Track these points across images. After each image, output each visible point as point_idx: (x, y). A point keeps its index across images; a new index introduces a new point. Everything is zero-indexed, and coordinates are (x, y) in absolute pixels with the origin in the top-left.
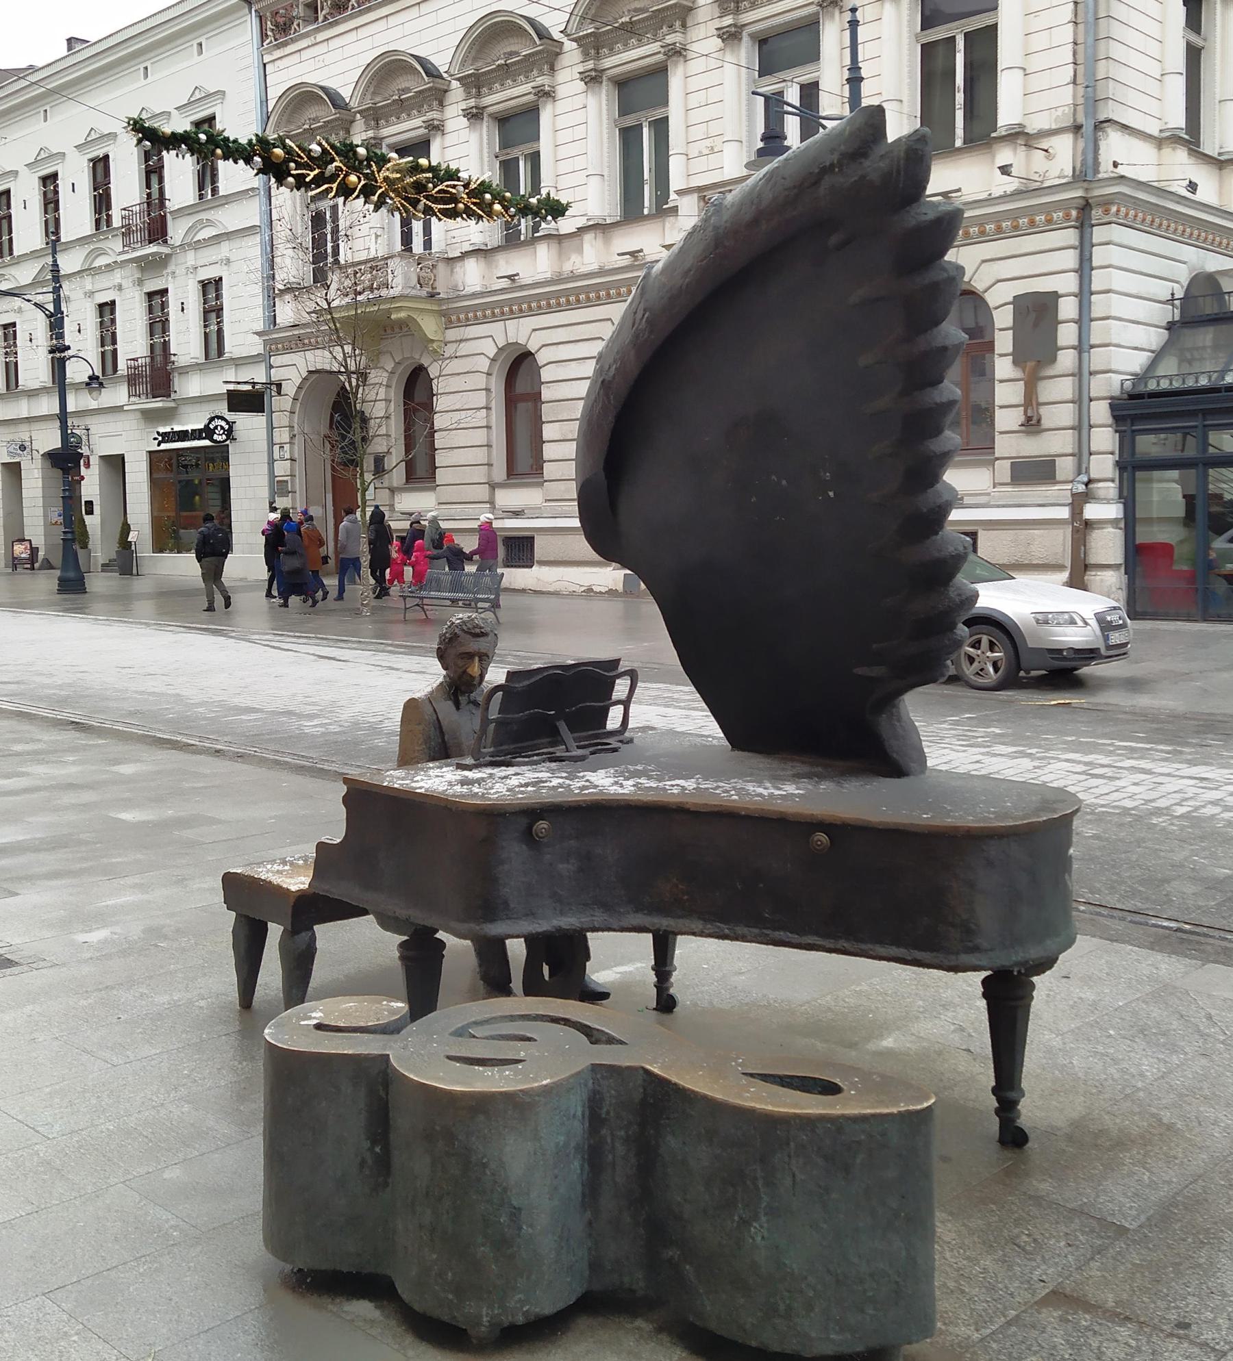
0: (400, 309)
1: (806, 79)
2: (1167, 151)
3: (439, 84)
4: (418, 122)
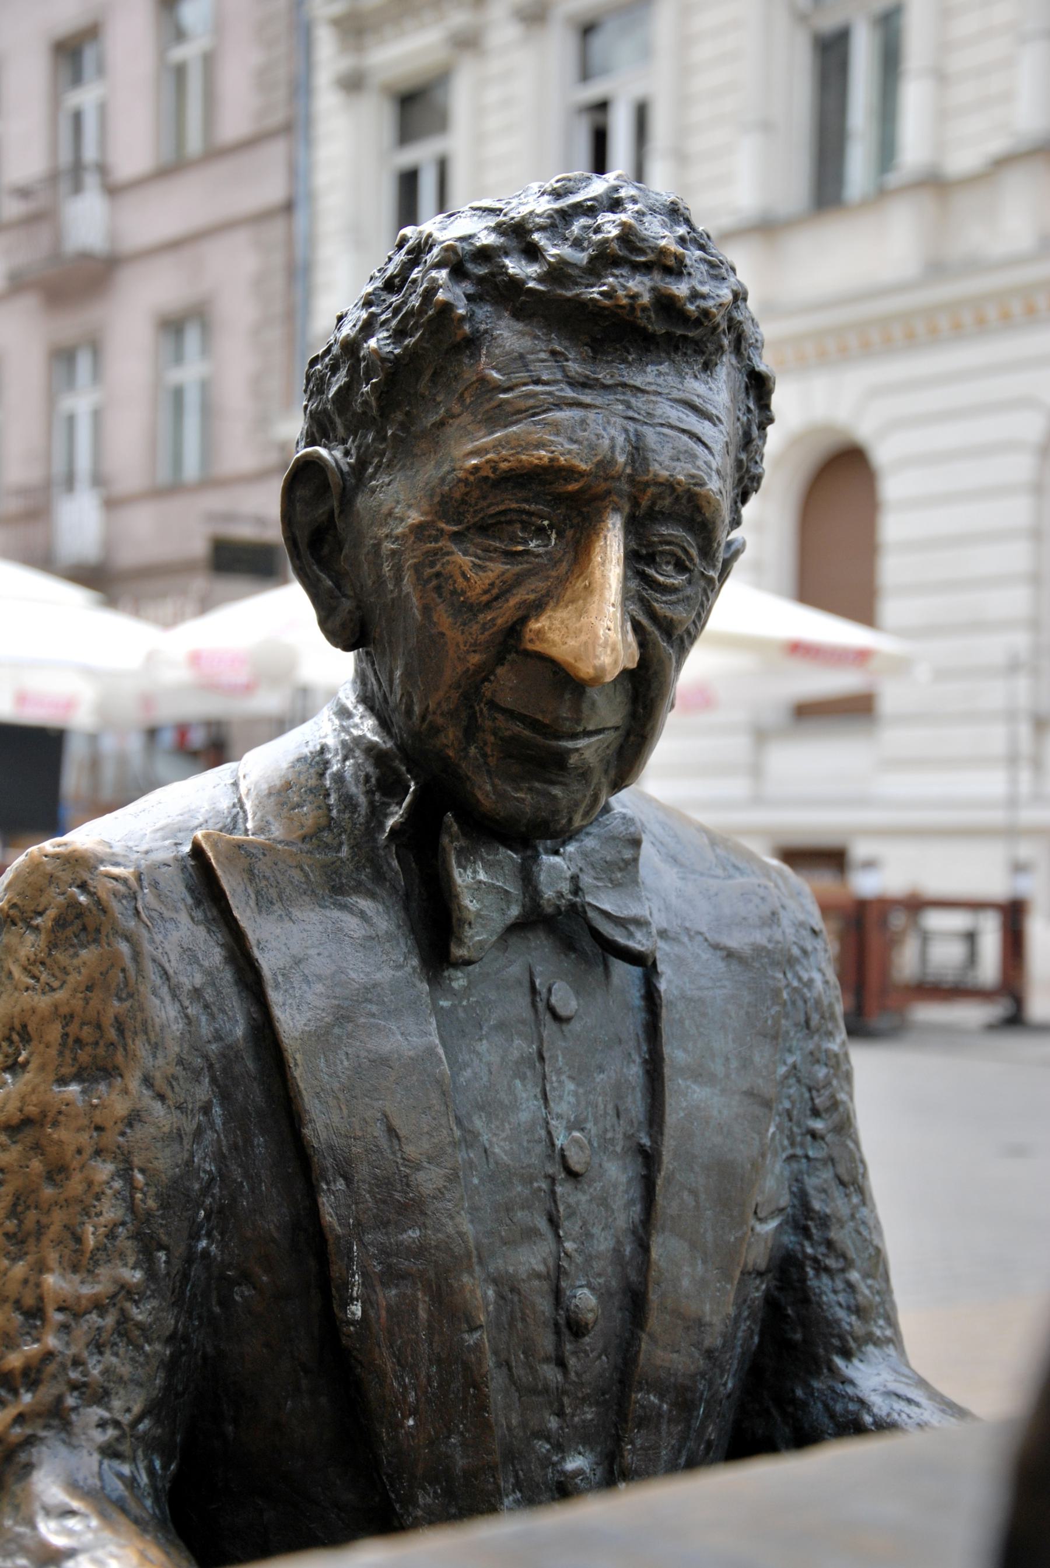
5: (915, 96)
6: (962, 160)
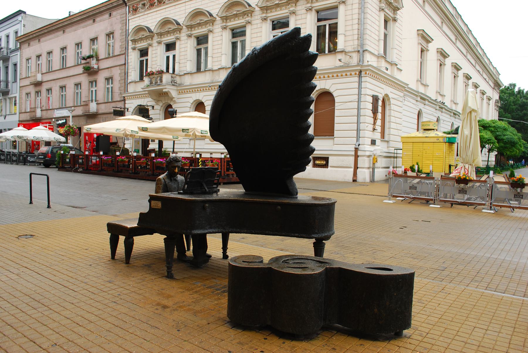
0: (166, 88)
1: (174, 54)
2: (380, 60)
3: (180, 27)
4: (173, 37)
5: (209, 59)
6: (215, 68)
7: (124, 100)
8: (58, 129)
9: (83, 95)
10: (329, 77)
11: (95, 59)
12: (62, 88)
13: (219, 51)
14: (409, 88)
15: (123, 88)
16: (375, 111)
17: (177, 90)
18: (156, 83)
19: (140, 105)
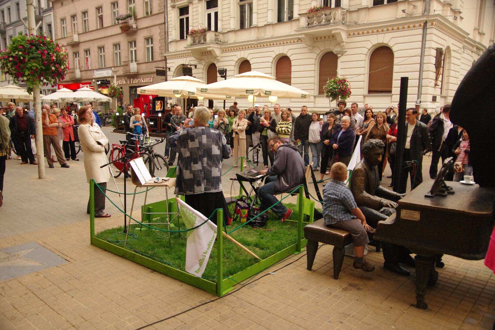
0: (210, 47)
1: (216, 11)
2: (446, 8)
5: (254, 16)
6: (260, 25)
7: (166, 60)
8: (100, 89)
9: (123, 56)
10: (388, 30)
11: (133, 18)
12: (101, 48)
13: (265, 6)
14: (469, 39)
15: (164, 48)
16: (438, 65)
17: (221, 49)
18: (199, 42)
19: (183, 65)
